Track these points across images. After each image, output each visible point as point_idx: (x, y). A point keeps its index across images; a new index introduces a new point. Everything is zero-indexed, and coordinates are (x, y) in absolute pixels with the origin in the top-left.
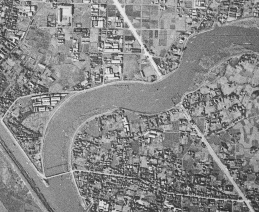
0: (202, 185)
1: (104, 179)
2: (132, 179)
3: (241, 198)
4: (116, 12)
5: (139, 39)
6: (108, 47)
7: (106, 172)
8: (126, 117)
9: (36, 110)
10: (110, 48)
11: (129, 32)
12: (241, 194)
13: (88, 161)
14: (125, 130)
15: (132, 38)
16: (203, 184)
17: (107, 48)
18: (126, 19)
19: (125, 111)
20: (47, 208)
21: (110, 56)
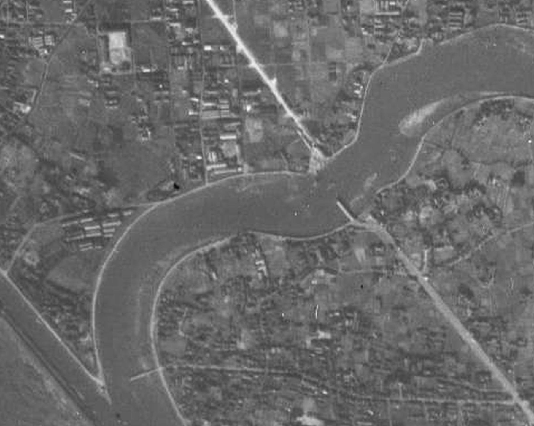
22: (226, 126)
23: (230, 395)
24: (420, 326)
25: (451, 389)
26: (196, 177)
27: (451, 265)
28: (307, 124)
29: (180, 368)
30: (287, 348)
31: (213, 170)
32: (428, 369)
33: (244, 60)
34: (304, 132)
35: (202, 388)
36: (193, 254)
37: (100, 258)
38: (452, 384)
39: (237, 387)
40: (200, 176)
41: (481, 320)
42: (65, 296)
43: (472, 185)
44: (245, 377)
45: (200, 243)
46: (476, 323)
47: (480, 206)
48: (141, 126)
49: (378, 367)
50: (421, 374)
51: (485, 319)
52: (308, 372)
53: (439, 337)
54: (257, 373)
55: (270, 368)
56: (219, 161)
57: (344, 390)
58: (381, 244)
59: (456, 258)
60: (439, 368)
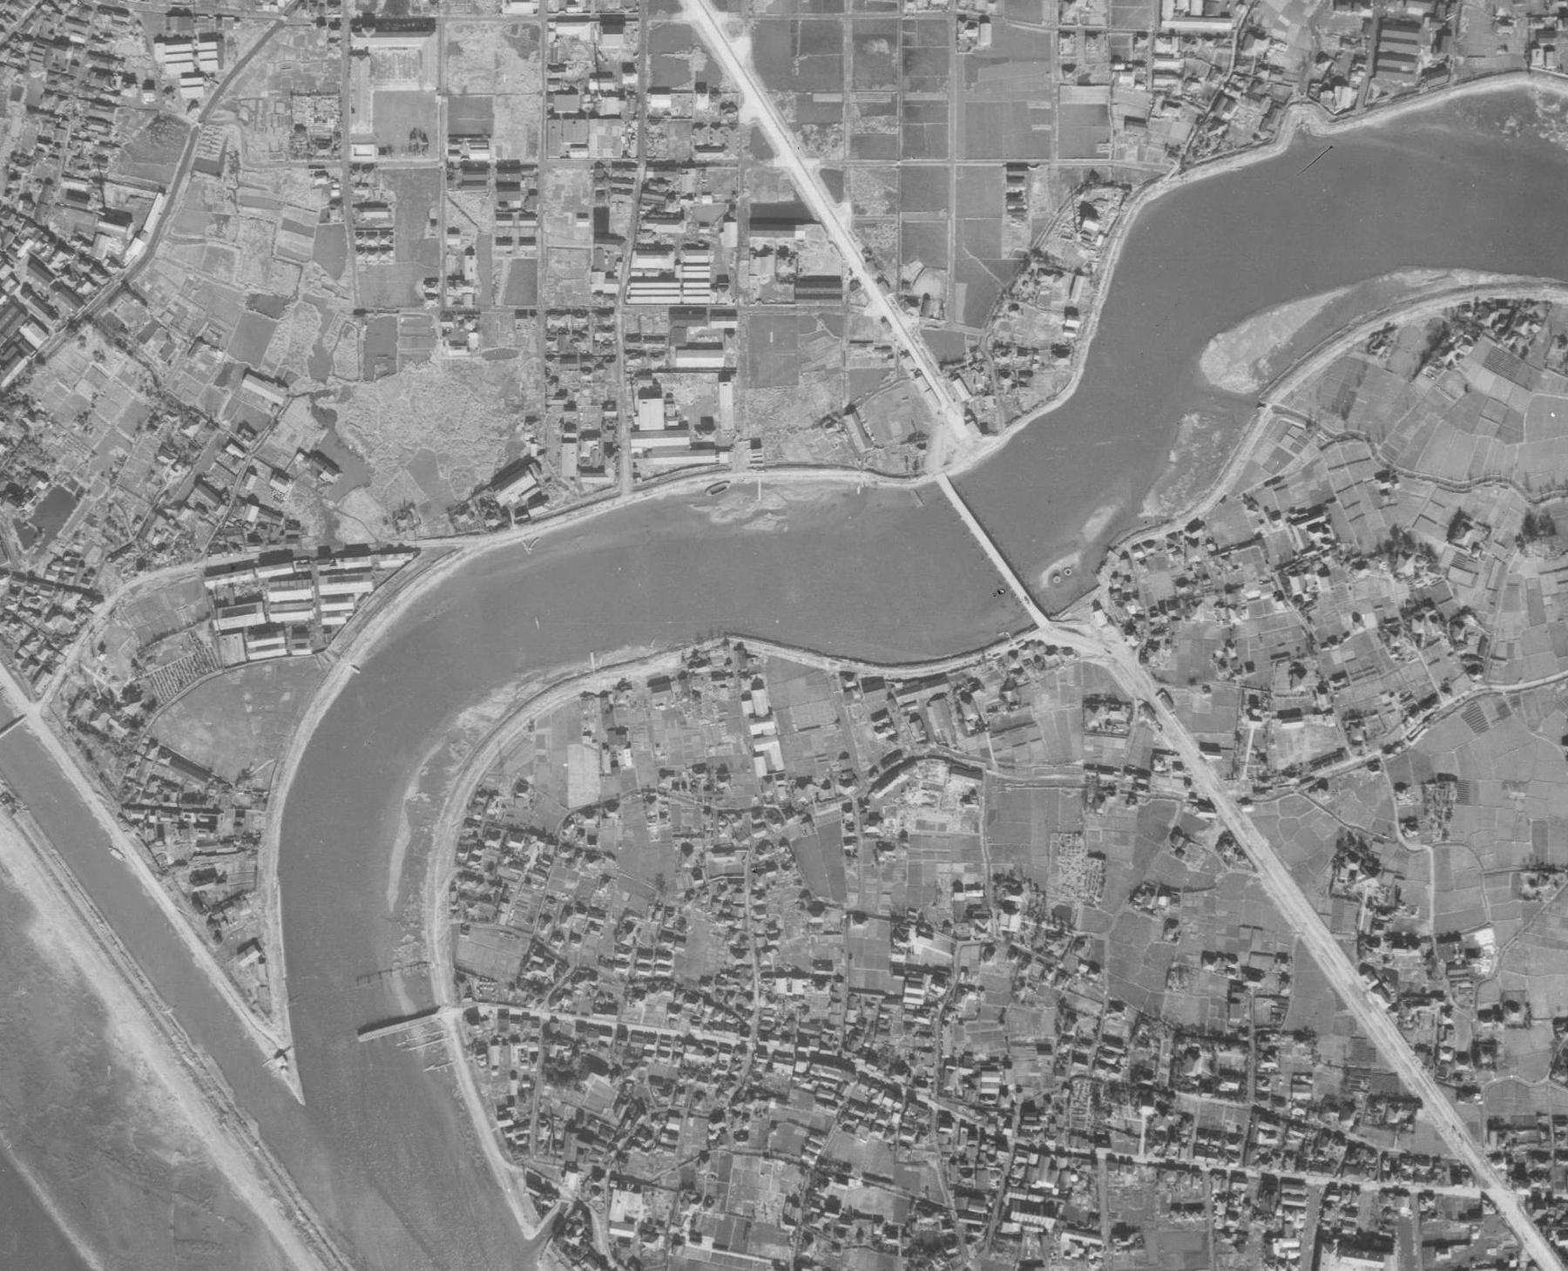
0: (1230, 1095)
1: (636, 1059)
2: (816, 1058)
3: (1460, 1174)
4: (697, 63)
5: (835, 217)
6: (656, 274)
7: (644, 1014)
8: (247, 371)
9: (276, 646)
10: (666, 276)
11: (775, 179)
12: (1465, 1151)
13: (541, 949)
14: (760, 763)
15: (794, 216)
16: (1234, 1086)
17: (643, 279)
18: (757, 107)
19: (752, 646)
20: (1330, 343)
21: (663, 329)
22: (693, 331)
23: (640, 1107)
24: (160, 377)
25: (1296, 1139)
26: (600, 471)
27: (1322, 773)
28: (930, 338)
29: (503, 1015)
30: (820, 982)
31: (647, 453)
32: (1229, 1074)
33: (760, 147)
34: (920, 358)
35: (561, 1075)
36: (569, 694)
37: (310, 677)
38: (1298, 1124)
39: (665, 1085)
40: (610, 471)
41: (1397, 940)
42: (197, 786)
43: (1398, 546)
44: (692, 1056)
45: (593, 664)
46: (1383, 948)
47: (1419, 606)
48: (447, 315)
49: (1081, 1059)
50: (1207, 1086)
51: (1412, 941)
52: (871, 1057)
53: (1268, 984)
54: (725, 1048)
55: (765, 1036)
56: (668, 428)
57: (978, 1121)
58: (1114, 702)
59: (1339, 755)
60: (1262, 1077)
